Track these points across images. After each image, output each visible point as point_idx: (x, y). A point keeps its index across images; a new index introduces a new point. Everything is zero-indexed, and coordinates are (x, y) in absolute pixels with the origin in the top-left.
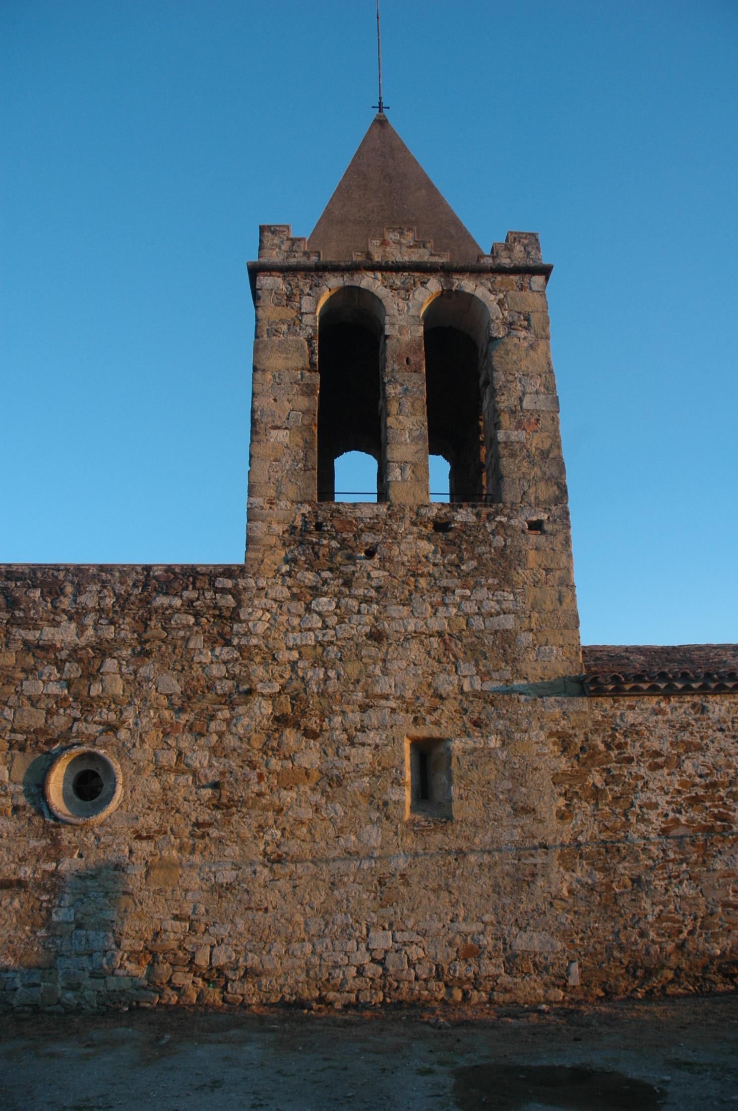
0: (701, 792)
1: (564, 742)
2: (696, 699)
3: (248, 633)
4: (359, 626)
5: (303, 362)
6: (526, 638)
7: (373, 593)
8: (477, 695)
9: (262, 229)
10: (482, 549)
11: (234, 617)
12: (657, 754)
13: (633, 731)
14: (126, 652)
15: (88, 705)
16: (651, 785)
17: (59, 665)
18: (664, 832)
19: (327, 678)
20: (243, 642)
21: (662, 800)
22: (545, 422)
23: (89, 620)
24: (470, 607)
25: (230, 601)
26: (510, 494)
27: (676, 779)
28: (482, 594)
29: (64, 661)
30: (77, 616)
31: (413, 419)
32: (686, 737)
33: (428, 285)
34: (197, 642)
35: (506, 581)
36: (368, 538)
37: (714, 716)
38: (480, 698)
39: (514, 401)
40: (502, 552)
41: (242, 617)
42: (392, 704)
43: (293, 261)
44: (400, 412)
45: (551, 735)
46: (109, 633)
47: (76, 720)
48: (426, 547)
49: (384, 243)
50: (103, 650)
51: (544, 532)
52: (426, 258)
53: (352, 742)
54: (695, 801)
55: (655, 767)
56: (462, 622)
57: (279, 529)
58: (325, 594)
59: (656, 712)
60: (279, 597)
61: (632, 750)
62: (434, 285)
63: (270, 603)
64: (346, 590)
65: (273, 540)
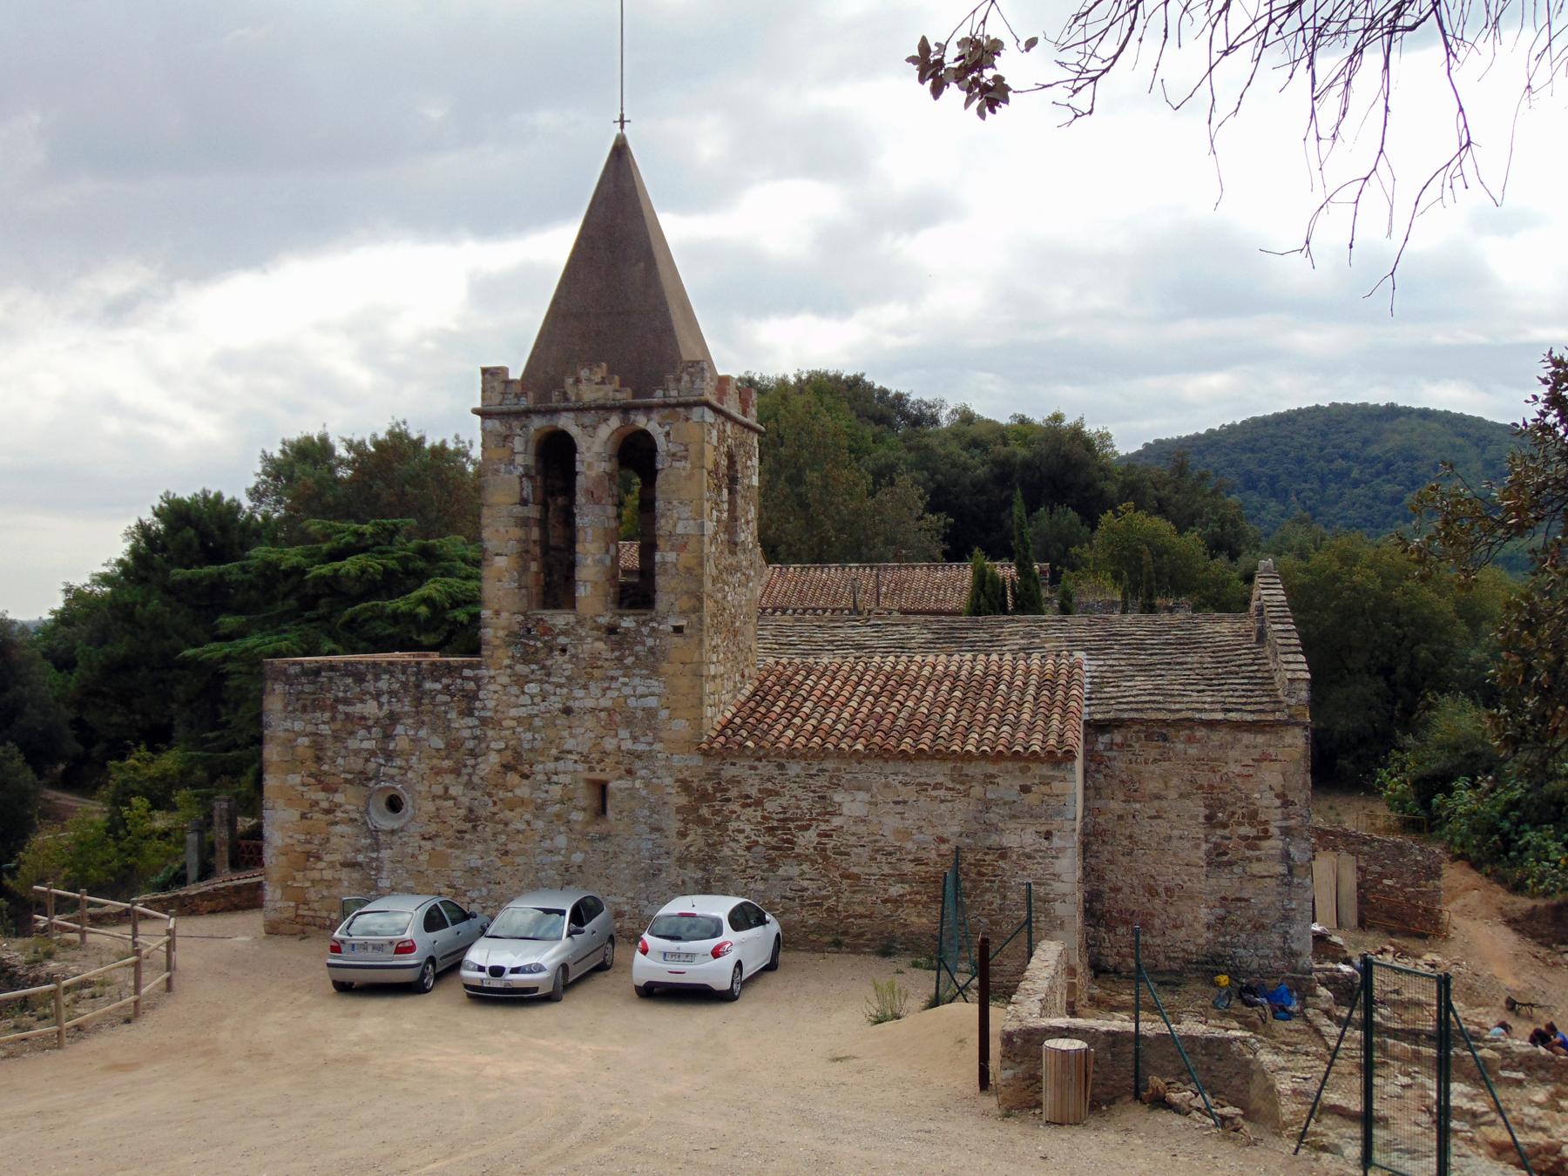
1: (685, 785)
4: (555, 703)
10: (638, 648)
11: (475, 697)
13: (735, 781)
15: (389, 756)
17: (369, 729)
18: (748, 849)
19: (534, 739)
21: (748, 828)
22: (693, 545)
23: (384, 699)
24: (627, 691)
25: (472, 685)
27: (759, 814)
28: (637, 681)
29: (371, 727)
32: (769, 785)
34: (453, 715)
36: (562, 640)
38: (1022, 533)
39: (669, 527)
40: (651, 651)
42: (575, 757)
43: (504, 408)
44: (584, 541)
48: (600, 645)
49: (578, 381)
50: (394, 718)
53: (549, 781)
54: (771, 830)
55: (745, 806)
56: (622, 700)
57: (501, 633)
58: (532, 682)
62: (615, 422)
63: (499, 688)
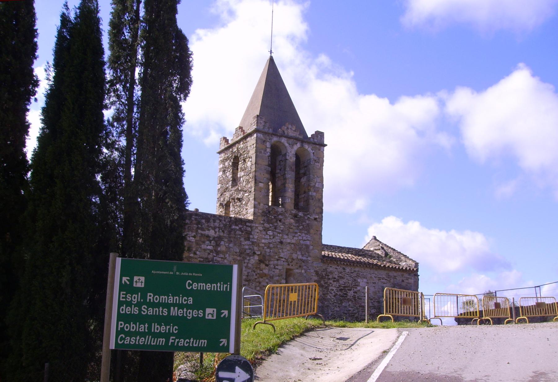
0: (342, 288)
2: (344, 267)
3: (253, 238)
4: (277, 239)
5: (267, 164)
6: (311, 247)
7: (280, 231)
8: (301, 260)
9: (429, 299)
12: (335, 278)
13: (331, 273)
14: (226, 240)
15: (218, 253)
16: (333, 285)
17: (210, 241)
18: (334, 296)
20: (253, 240)
21: (335, 289)
26: (311, 210)
30: (214, 228)
31: (292, 185)
33: (297, 145)
34: (242, 239)
35: (308, 233)
37: (347, 271)
39: (314, 184)
40: (308, 224)
41: (252, 234)
42: (283, 260)
45: (315, 271)
46: (222, 234)
47: (214, 256)
48: (292, 221)
51: (317, 221)
52: (298, 136)
53: (275, 268)
54: (341, 290)
55: (334, 281)
57: (260, 211)
59: (336, 269)
60: (261, 229)
61: (330, 277)
64: (275, 230)
65: (259, 214)
